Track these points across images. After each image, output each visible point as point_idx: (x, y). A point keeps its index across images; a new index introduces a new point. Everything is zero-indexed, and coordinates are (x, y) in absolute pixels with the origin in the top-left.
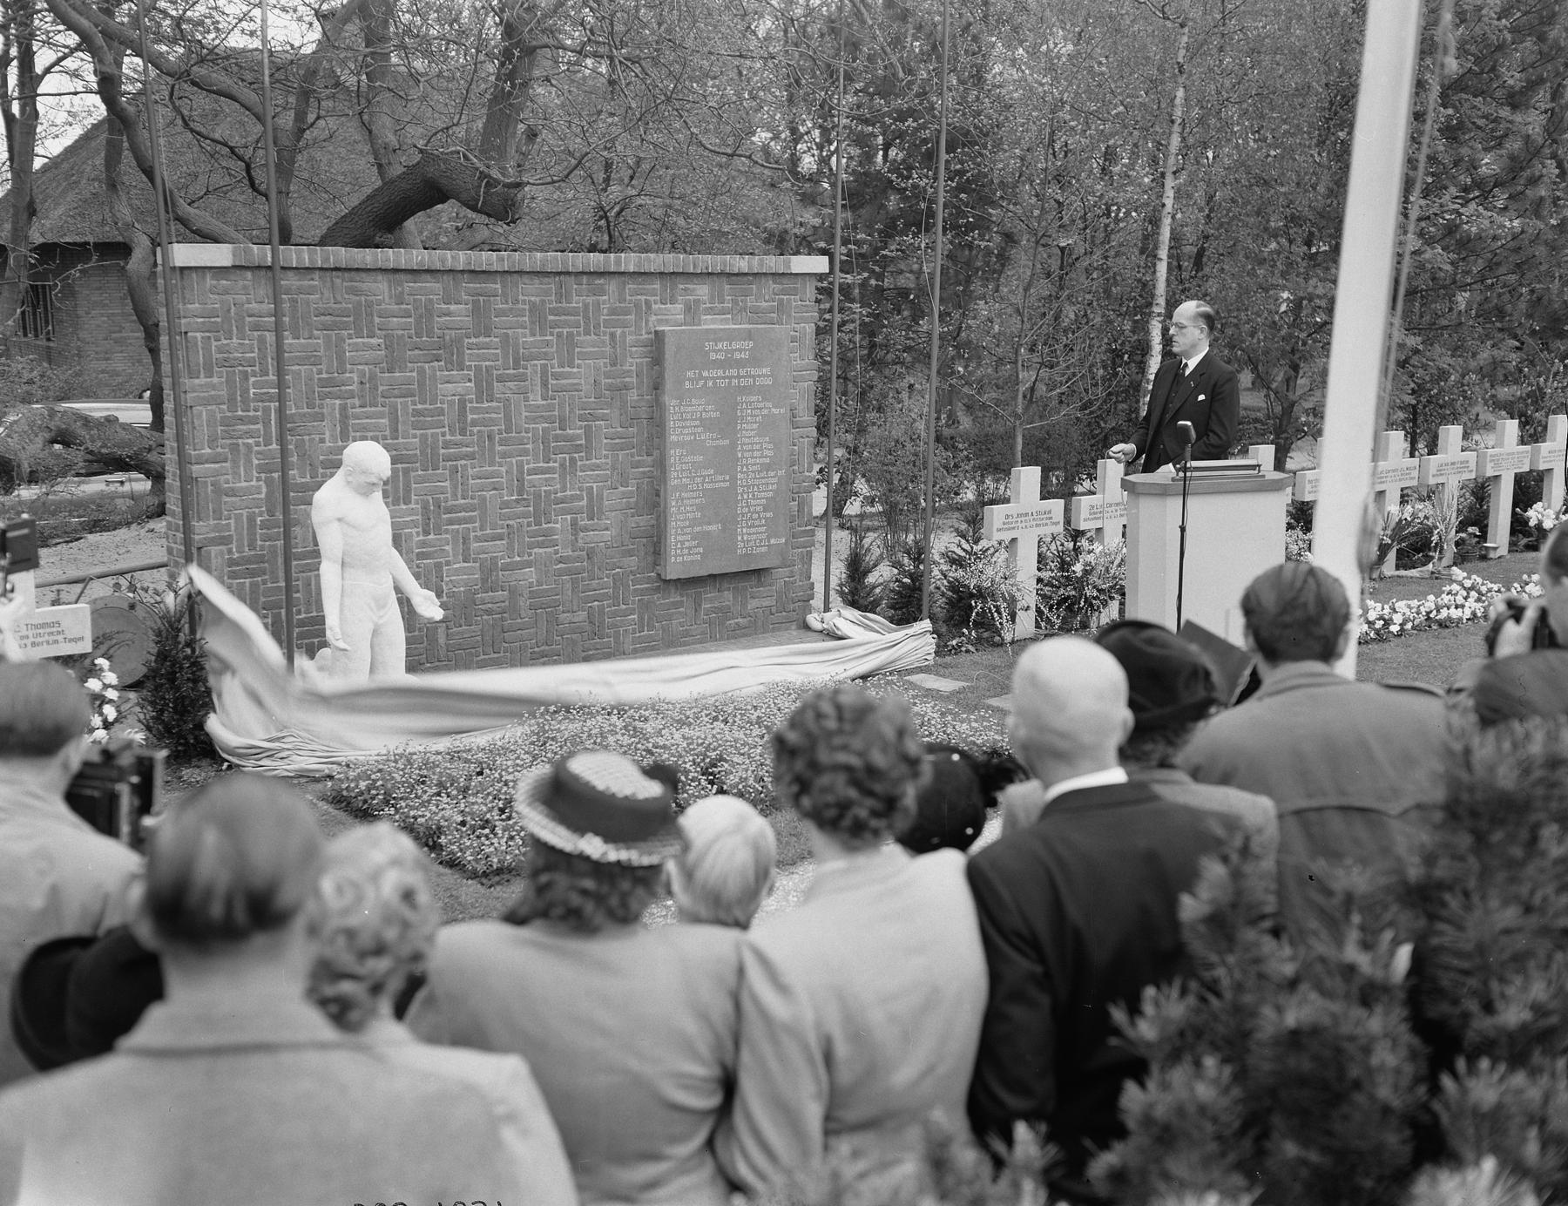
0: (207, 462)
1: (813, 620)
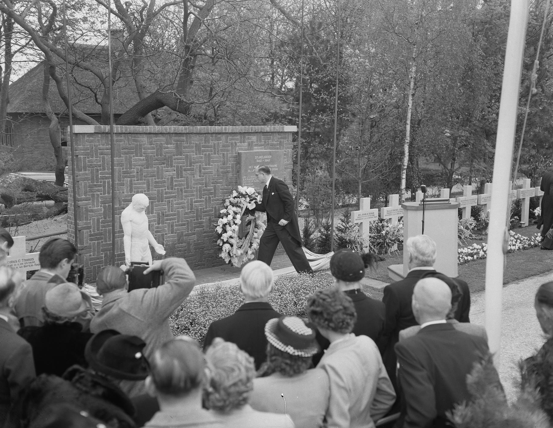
0: (83, 201)
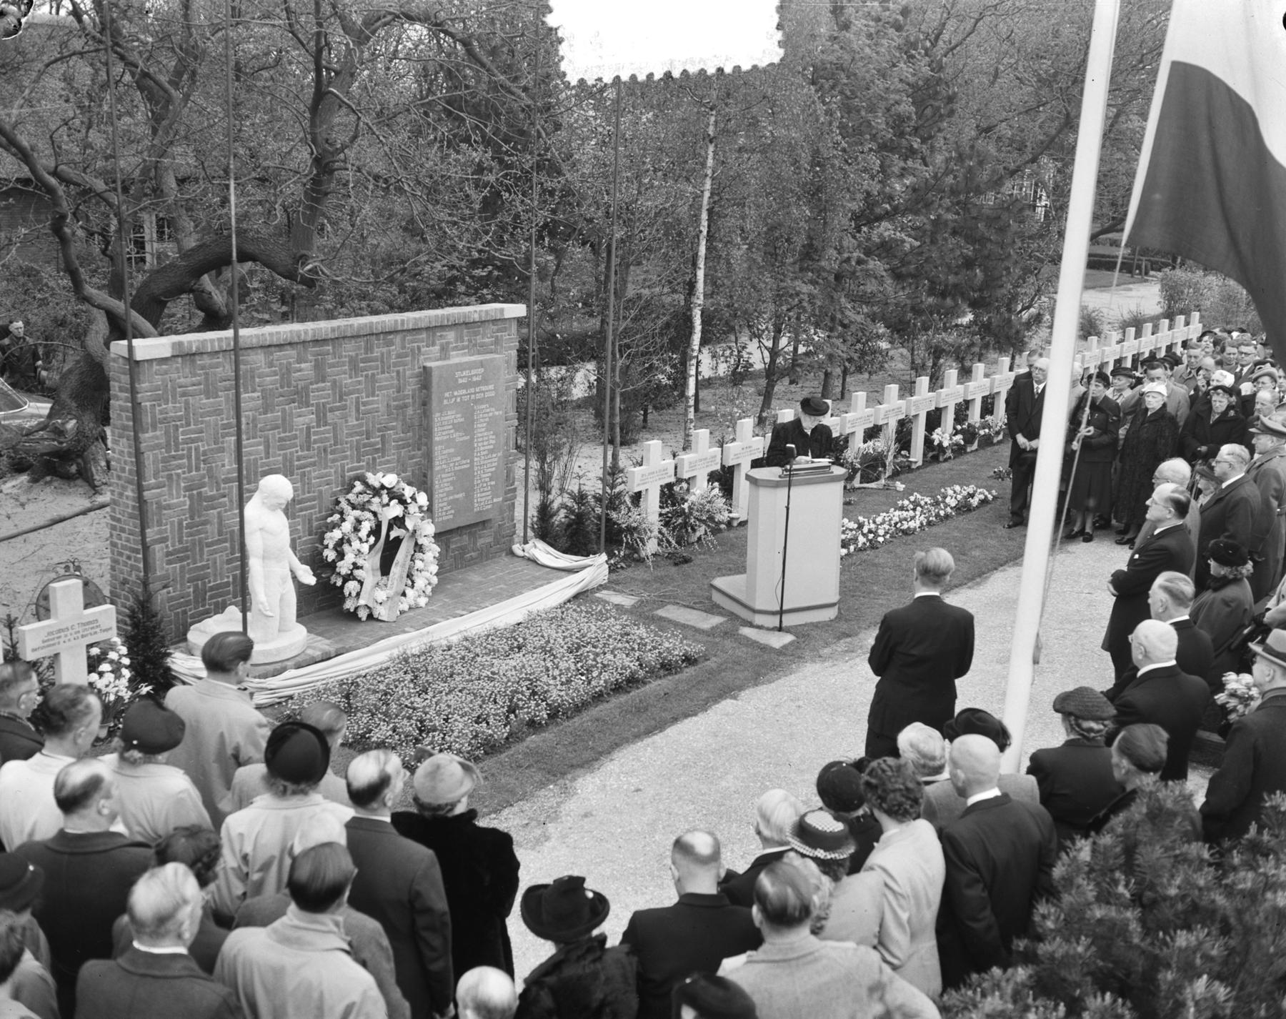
1: (517, 548)
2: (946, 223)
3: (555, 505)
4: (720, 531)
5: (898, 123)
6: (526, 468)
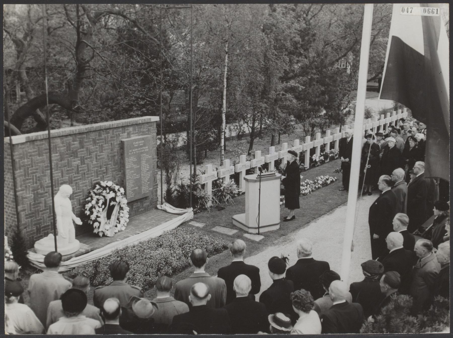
1: (159, 206)
2: (314, 79)
3: (173, 189)
4: (235, 197)
5: (295, 44)
6: (161, 175)
